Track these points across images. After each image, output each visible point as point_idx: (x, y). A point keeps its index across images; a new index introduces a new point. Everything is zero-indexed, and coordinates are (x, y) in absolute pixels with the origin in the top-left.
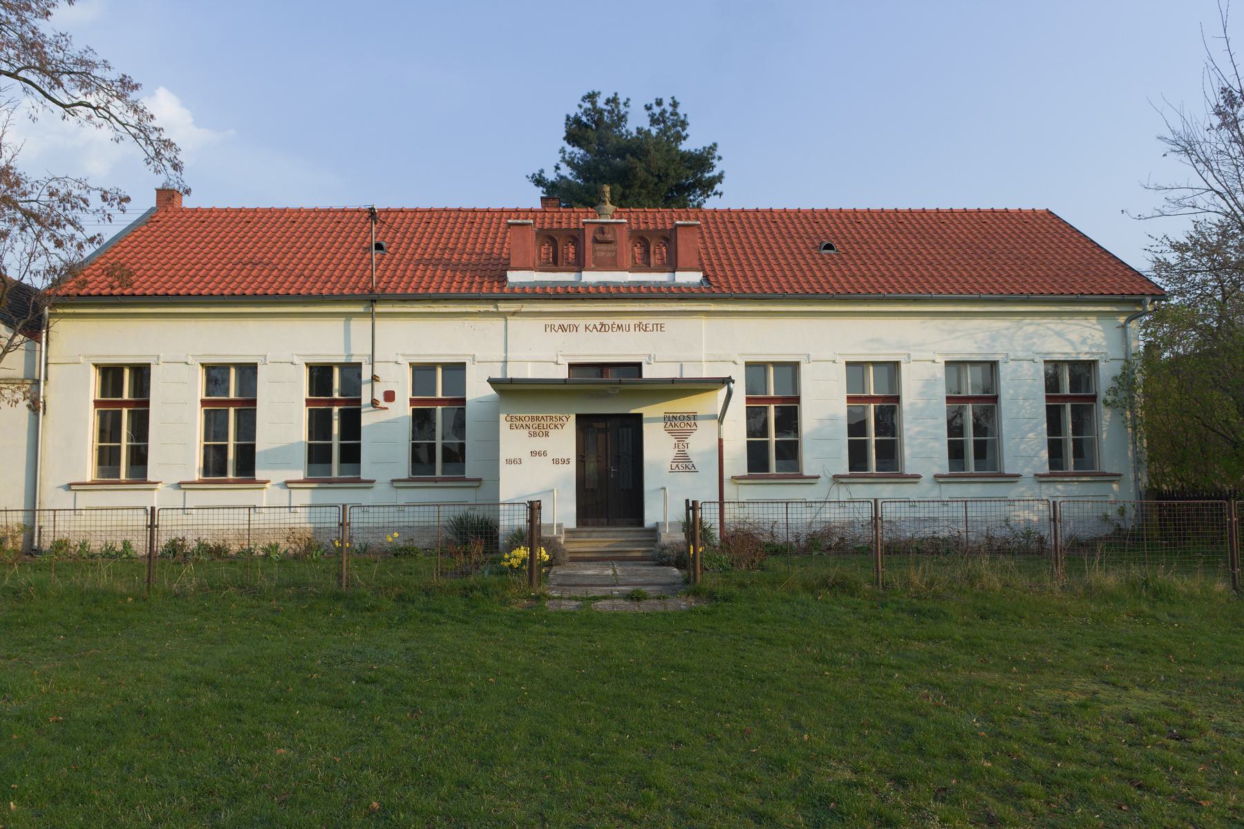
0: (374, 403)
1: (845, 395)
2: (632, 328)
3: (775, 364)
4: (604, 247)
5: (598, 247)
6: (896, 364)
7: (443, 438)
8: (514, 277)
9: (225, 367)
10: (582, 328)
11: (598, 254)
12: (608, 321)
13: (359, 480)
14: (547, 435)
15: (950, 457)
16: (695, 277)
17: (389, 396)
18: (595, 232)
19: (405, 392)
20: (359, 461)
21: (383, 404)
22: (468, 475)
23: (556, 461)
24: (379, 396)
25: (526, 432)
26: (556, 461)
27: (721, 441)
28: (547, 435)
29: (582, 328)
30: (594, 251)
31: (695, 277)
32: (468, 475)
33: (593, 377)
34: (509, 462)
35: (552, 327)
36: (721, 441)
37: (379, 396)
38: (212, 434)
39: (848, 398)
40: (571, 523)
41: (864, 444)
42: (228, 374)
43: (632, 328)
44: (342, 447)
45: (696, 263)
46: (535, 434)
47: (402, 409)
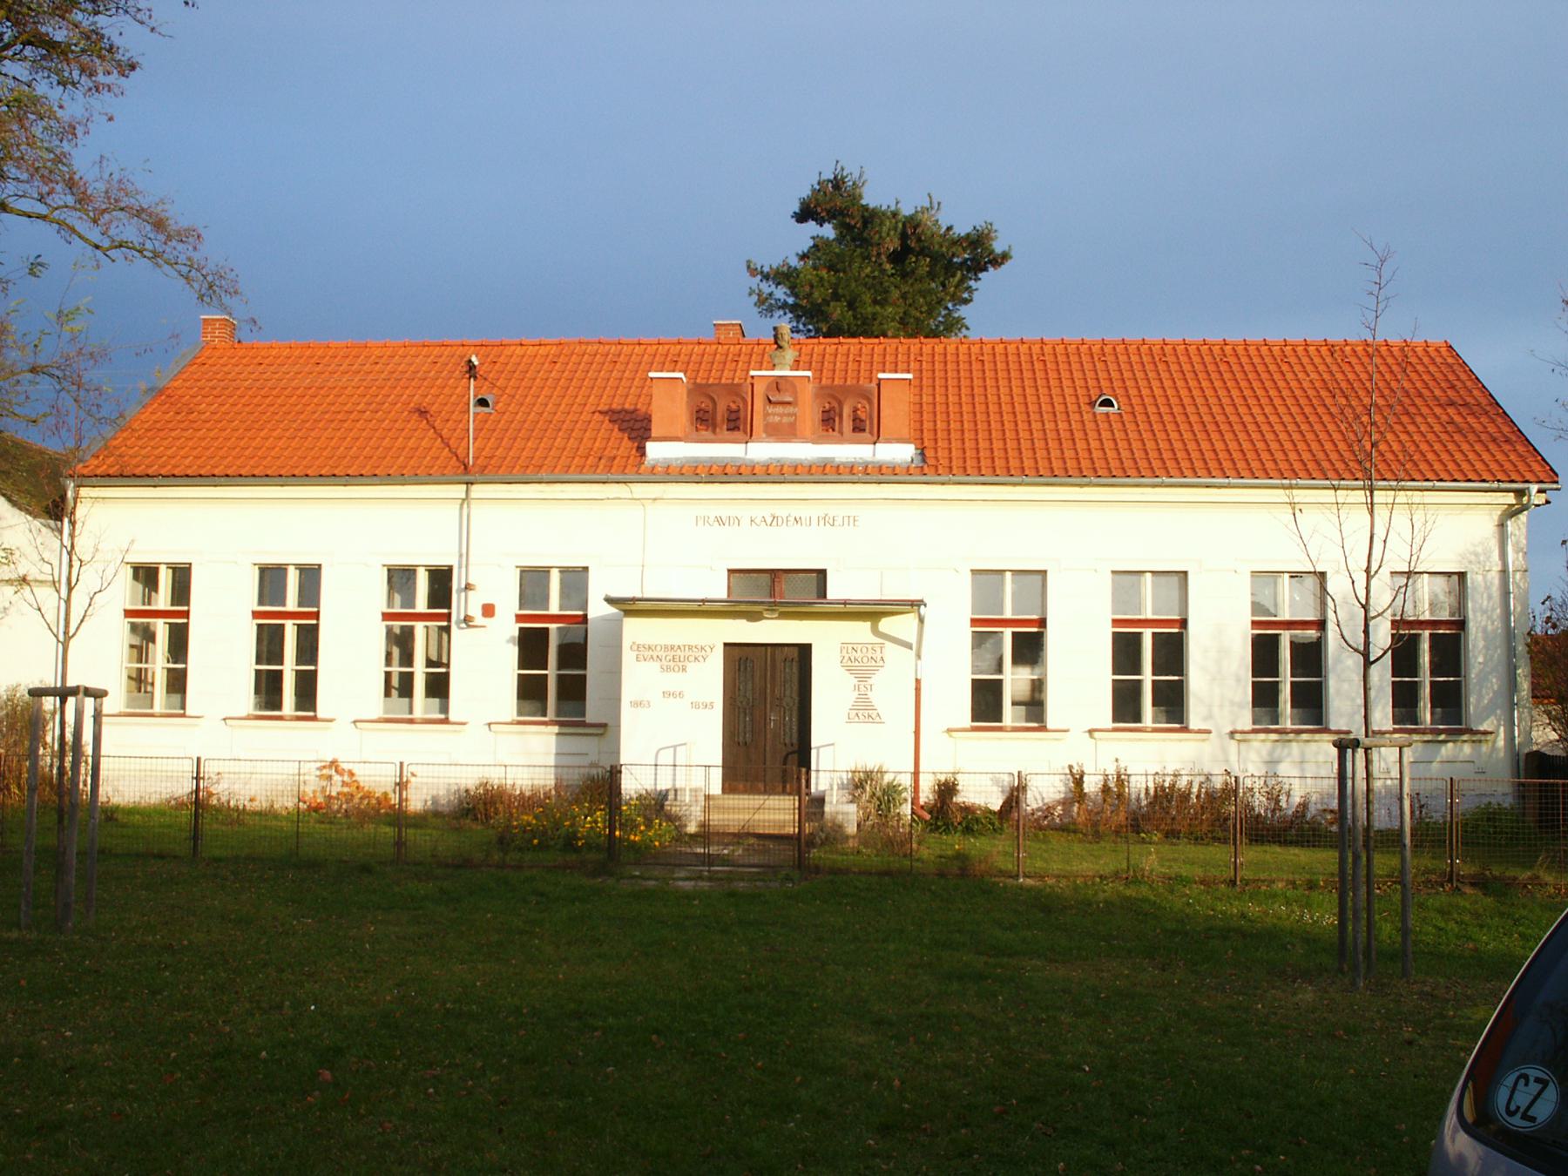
0: (467, 620)
1: (968, 615)
2: (815, 521)
3: (1015, 572)
4: (779, 409)
5: (770, 409)
6: (1185, 573)
7: (561, 668)
8: (656, 451)
9: (544, 572)
10: (745, 521)
11: (771, 419)
12: (782, 511)
13: (583, 724)
14: (684, 670)
15: (519, 697)
16: (903, 453)
17: (488, 610)
18: (768, 388)
19: (509, 604)
20: (584, 699)
21: (479, 619)
22: (589, 718)
23: (695, 705)
24: (475, 611)
25: (657, 665)
26: (695, 705)
27: (918, 681)
28: (684, 670)
29: (745, 521)
30: (766, 415)
31: (903, 453)
32: (589, 718)
33: (770, 589)
34: (636, 704)
35: (706, 520)
36: (918, 681)
37: (475, 611)
38: (264, 656)
39: (1253, 623)
40: (716, 788)
41: (277, 677)
42: (1002, 583)
43: (815, 521)
44: (560, 678)
45: (905, 432)
46: (668, 669)
47: (505, 628)
